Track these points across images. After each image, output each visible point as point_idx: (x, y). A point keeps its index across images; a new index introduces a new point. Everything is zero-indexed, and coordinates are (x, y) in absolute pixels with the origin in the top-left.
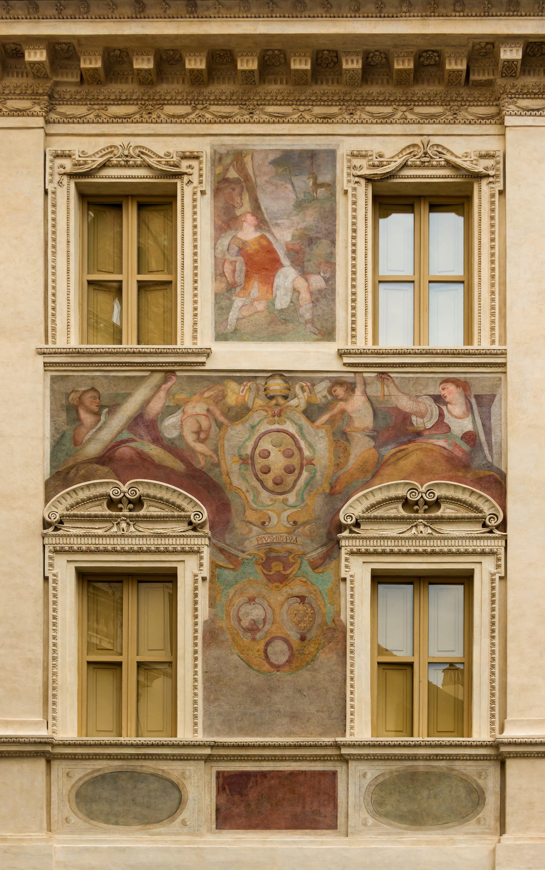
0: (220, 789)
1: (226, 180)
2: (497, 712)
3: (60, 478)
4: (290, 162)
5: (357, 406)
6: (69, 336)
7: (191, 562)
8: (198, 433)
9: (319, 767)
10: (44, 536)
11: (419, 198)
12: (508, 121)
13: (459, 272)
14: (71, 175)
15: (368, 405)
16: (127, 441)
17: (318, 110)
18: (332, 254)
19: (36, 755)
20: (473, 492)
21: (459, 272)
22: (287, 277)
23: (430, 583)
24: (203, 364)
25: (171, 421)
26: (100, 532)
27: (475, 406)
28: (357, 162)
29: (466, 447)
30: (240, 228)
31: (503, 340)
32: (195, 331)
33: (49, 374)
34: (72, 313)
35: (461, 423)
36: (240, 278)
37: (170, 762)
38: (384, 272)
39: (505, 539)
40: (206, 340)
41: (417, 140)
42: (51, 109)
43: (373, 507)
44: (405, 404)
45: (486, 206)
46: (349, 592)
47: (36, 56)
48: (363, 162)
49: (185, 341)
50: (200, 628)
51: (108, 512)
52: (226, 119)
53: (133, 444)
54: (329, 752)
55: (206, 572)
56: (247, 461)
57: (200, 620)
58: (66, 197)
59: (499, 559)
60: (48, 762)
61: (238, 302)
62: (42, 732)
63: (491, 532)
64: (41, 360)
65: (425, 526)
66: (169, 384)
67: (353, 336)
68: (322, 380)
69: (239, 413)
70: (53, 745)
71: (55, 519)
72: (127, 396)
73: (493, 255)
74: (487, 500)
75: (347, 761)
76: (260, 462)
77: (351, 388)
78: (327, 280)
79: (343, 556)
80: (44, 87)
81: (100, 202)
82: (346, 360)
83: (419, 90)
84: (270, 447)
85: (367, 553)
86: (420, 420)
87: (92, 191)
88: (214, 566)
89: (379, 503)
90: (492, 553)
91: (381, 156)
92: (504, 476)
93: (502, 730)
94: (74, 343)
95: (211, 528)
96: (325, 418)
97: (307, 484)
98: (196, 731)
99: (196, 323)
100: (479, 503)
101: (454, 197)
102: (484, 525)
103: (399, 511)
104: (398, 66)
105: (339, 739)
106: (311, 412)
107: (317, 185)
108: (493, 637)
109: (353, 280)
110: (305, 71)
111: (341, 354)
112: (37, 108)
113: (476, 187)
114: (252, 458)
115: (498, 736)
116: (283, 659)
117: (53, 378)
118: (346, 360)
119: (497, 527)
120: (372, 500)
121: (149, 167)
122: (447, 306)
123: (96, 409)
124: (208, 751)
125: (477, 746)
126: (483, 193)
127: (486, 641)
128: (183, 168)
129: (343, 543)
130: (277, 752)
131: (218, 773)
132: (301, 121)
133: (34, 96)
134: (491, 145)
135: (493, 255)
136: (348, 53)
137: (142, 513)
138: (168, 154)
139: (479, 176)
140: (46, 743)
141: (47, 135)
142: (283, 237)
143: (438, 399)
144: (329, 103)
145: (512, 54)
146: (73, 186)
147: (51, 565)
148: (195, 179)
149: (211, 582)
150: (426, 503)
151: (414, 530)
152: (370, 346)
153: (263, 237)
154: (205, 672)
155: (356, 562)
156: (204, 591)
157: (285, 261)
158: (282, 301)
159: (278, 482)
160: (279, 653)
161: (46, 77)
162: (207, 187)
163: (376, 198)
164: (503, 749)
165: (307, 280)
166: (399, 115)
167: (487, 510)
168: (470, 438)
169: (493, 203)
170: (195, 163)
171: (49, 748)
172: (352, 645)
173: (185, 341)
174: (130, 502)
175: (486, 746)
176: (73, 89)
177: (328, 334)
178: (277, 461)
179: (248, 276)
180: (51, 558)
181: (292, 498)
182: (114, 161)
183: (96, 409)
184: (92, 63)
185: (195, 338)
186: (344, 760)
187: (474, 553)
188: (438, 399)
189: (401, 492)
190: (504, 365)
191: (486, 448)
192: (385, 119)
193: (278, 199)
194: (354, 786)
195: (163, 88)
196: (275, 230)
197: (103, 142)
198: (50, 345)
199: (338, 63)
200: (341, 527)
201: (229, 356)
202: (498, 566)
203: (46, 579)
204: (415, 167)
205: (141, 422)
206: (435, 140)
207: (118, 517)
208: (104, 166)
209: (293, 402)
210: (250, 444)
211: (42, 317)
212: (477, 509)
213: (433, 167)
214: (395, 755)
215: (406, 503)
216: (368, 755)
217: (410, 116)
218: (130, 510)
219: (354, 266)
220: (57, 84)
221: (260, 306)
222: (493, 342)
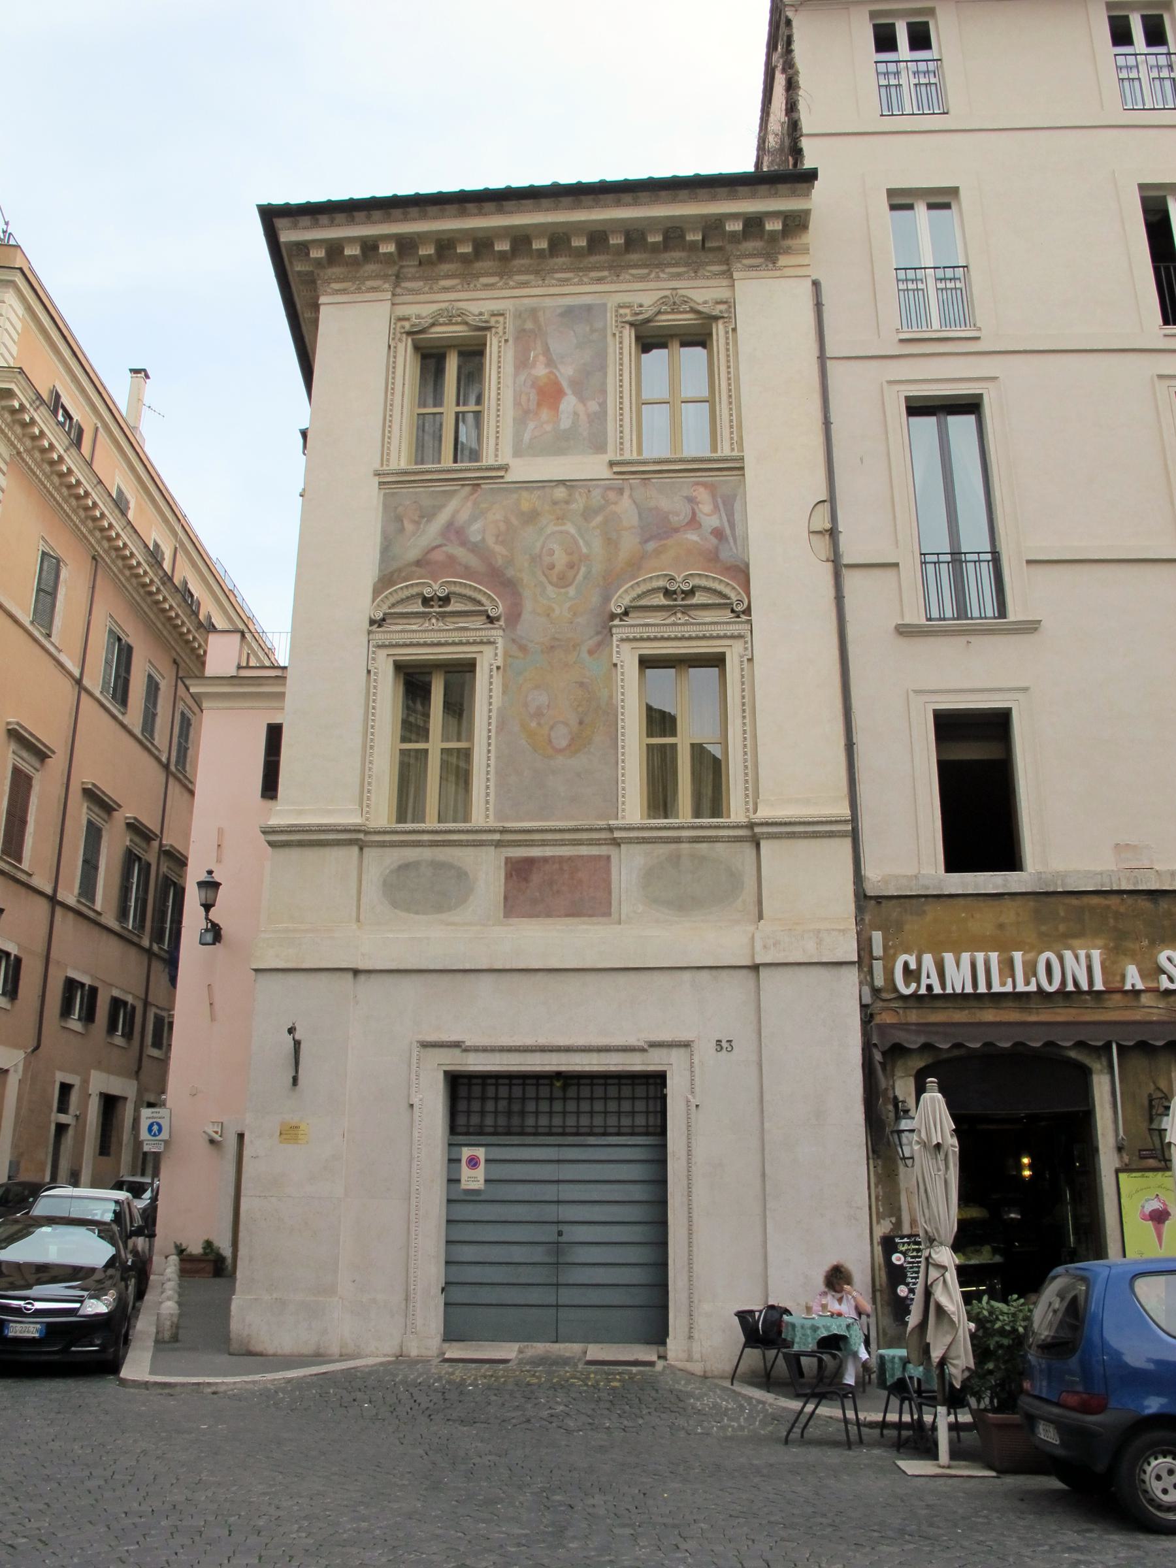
0: (508, 876)
1: (524, 330)
2: (750, 792)
3: (385, 582)
4: (569, 314)
5: (625, 507)
6: (401, 460)
7: (488, 650)
8: (498, 536)
9: (594, 851)
10: (369, 632)
11: (672, 336)
12: (736, 275)
13: (705, 393)
14: (409, 333)
15: (633, 506)
16: (440, 546)
17: (593, 274)
18: (604, 384)
19: (350, 842)
20: (721, 581)
21: (705, 393)
22: (569, 403)
23: (691, 667)
24: (502, 477)
26: (414, 627)
27: (721, 506)
28: (622, 311)
29: (714, 541)
30: (534, 365)
31: (741, 449)
32: (497, 450)
33: (383, 492)
34: (403, 440)
35: (711, 521)
36: (533, 406)
37: (464, 849)
38: (645, 396)
39: (750, 622)
40: (505, 457)
41: (668, 293)
42: (396, 285)
43: (639, 597)
44: (664, 503)
45: (722, 341)
46: (620, 677)
47: (388, 248)
48: (627, 311)
49: (488, 459)
50: (494, 714)
51: (422, 609)
52: (525, 284)
53: (444, 549)
54: (603, 835)
55: (500, 663)
56: (535, 559)
57: (494, 707)
58: (405, 350)
59: (746, 643)
60: (361, 849)
61: (531, 425)
62: (354, 820)
63: (738, 617)
64: (376, 480)
65: (683, 613)
66: (476, 495)
67: (621, 449)
68: (598, 486)
69: (531, 517)
70: (366, 833)
71: (379, 615)
72: (440, 507)
73: (729, 379)
74: (734, 588)
75: (619, 845)
76: (547, 560)
77: (621, 491)
78: (600, 405)
79: (615, 643)
80: (392, 271)
81: (431, 358)
82: (616, 469)
83: (667, 256)
84: (555, 547)
85: (635, 639)
86: (676, 518)
87: (423, 344)
88: (506, 654)
89: (644, 593)
90: (740, 637)
91: (641, 306)
92: (747, 565)
93: (755, 811)
94: (403, 465)
95: (506, 621)
96: (599, 519)
97: (585, 578)
98: (487, 816)
99: (499, 443)
100: (726, 591)
101: (699, 337)
102: (733, 611)
103: (660, 600)
104: (651, 239)
105: (611, 822)
106: (588, 513)
107: (593, 331)
108: (744, 717)
109: (621, 403)
110: (582, 247)
111: (612, 464)
112: (387, 286)
113: (714, 326)
114: (540, 556)
115: (752, 816)
116: (564, 743)
117: (385, 494)
118: (616, 469)
119: (743, 612)
120: (639, 591)
121: (466, 323)
122: (694, 418)
123: (417, 518)
124: (497, 837)
125: (734, 827)
126: (719, 331)
127: (739, 721)
128: (492, 323)
129: (614, 630)
130: (558, 836)
131: (507, 858)
132: (581, 283)
133: (385, 277)
134: (724, 294)
135: (729, 379)
136: (613, 232)
137: (448, 609)
138: (481, 314)
139: (716, 318)
140: (359, 831)
141: (393, 304)
142: (566, 372)
143: (691, 500)
144: (602, 269)
145: (736, 226)
146: (410, 340)
147: (374, 659)
148: (500, 330)
149: (505, 670)
150: (683, 592)
151: (673, 618)
152: (635, 456)
153: (551, 372)
154: (497, 758)
155: (626, 646)
156: (497, 680)
157: (568, 391)
158: (565, 423)
160: (561, 738)
161: (395, 263)
162: (510, 336)
163: (638, 338)
164: (757, 830)
165: (585, 405)
166: (652, 276)
167: (733, 596)
168: (718, 533)
169: (727, 338)
170: (501, 319)
171: (361, 836)
172: (623, 728)
173: (488, 459)
174: (440, 599)
175: (742, 827)
176: (413, 270)
177: (601, 448)
178: (560, 559)
179: (539, 405)
180: (374, 652)
181: (572, 591)
182: (441, 320)
183: (417, 518)
184: (427, 250)
185: (496, 456)
186: (616, 843)
187: (725, 637)
188: (691, 500)
189: (661, 583)
190: (742, 468)
191: (731, 540)
192: (642, 279)
194: (628, 869)
195: (479, 265)
196: (559, 366)
197: (435, 307)
198: (385, 467)
199: (606, 240)
200: (613, 616)
201: (522, 470)
202: (746, 649)
203: (369, 672)
204: (666, 313)
205: (454, 531)
206: (681, 292)
207: (430, 613)
208: (433, 325)
209: (574, 506)
210: (539, 545)
211: (380, 444)
212: (726, 597)
213: (681, 313)
214: (661, 838)
215: (667, 593)
216: (637, 838)
217: (662, 275)
218: (440, 606)
219: (621, 392)
220: (402, 267)
221: (548, 428)
222: (733, 450)
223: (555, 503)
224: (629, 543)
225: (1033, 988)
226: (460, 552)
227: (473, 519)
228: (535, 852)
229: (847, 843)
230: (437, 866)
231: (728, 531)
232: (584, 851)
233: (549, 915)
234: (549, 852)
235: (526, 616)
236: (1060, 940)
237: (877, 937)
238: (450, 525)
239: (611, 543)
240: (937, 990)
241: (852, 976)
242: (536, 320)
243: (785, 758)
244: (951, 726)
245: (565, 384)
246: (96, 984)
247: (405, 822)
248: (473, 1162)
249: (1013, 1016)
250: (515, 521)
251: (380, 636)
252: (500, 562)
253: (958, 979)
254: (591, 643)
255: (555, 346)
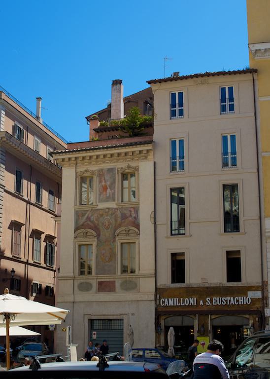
0: (99, 285)
3: (76, 229)
9: (113, 280)
22: (109, 191)
25: (92, 217)
35: (134, 215)
56: (103, 224)
61: (102, 195)
76: (105, 224)
77: (118, 209)
96: (114, 215)
106: (112, 214)
142: (108, 183)
157: (108, 188)
159: (107, 227)
168: (135, 218)
178: (107, 223)
181: (109, 230)
188: (130, 211)
189: (124, 229)
193: (107, 177)
205: (88, 218)
221: (105, 196)
223: (106, 212)
224: (119, 220)
225: (184, 305)
226: (89, 223)
227: (92, 216)
228: (103, 280)
229: (154, 278)
230: (86, 283)
231: (76, 288)
232: (111, 280)
233: (105, 291)
234: (105, 280)
235: (101, 235)
236: (189, 296)
237: (158, 296)
238: (88, 217)
239: (116, 220)
240: (168, 305)
241: (154, 302)
242: (103, 172)
243: (144, 261)
244: (174, 255)
245: (108, 186)
246: (41, 283)
247: (85, 271)
248: (94, 334)
249: (181, 310)
250: (99, 216)
251: (76, 240)
252: (96, 224)
253: (171, 303)
254: (112, 241)
255: (107, 178)
